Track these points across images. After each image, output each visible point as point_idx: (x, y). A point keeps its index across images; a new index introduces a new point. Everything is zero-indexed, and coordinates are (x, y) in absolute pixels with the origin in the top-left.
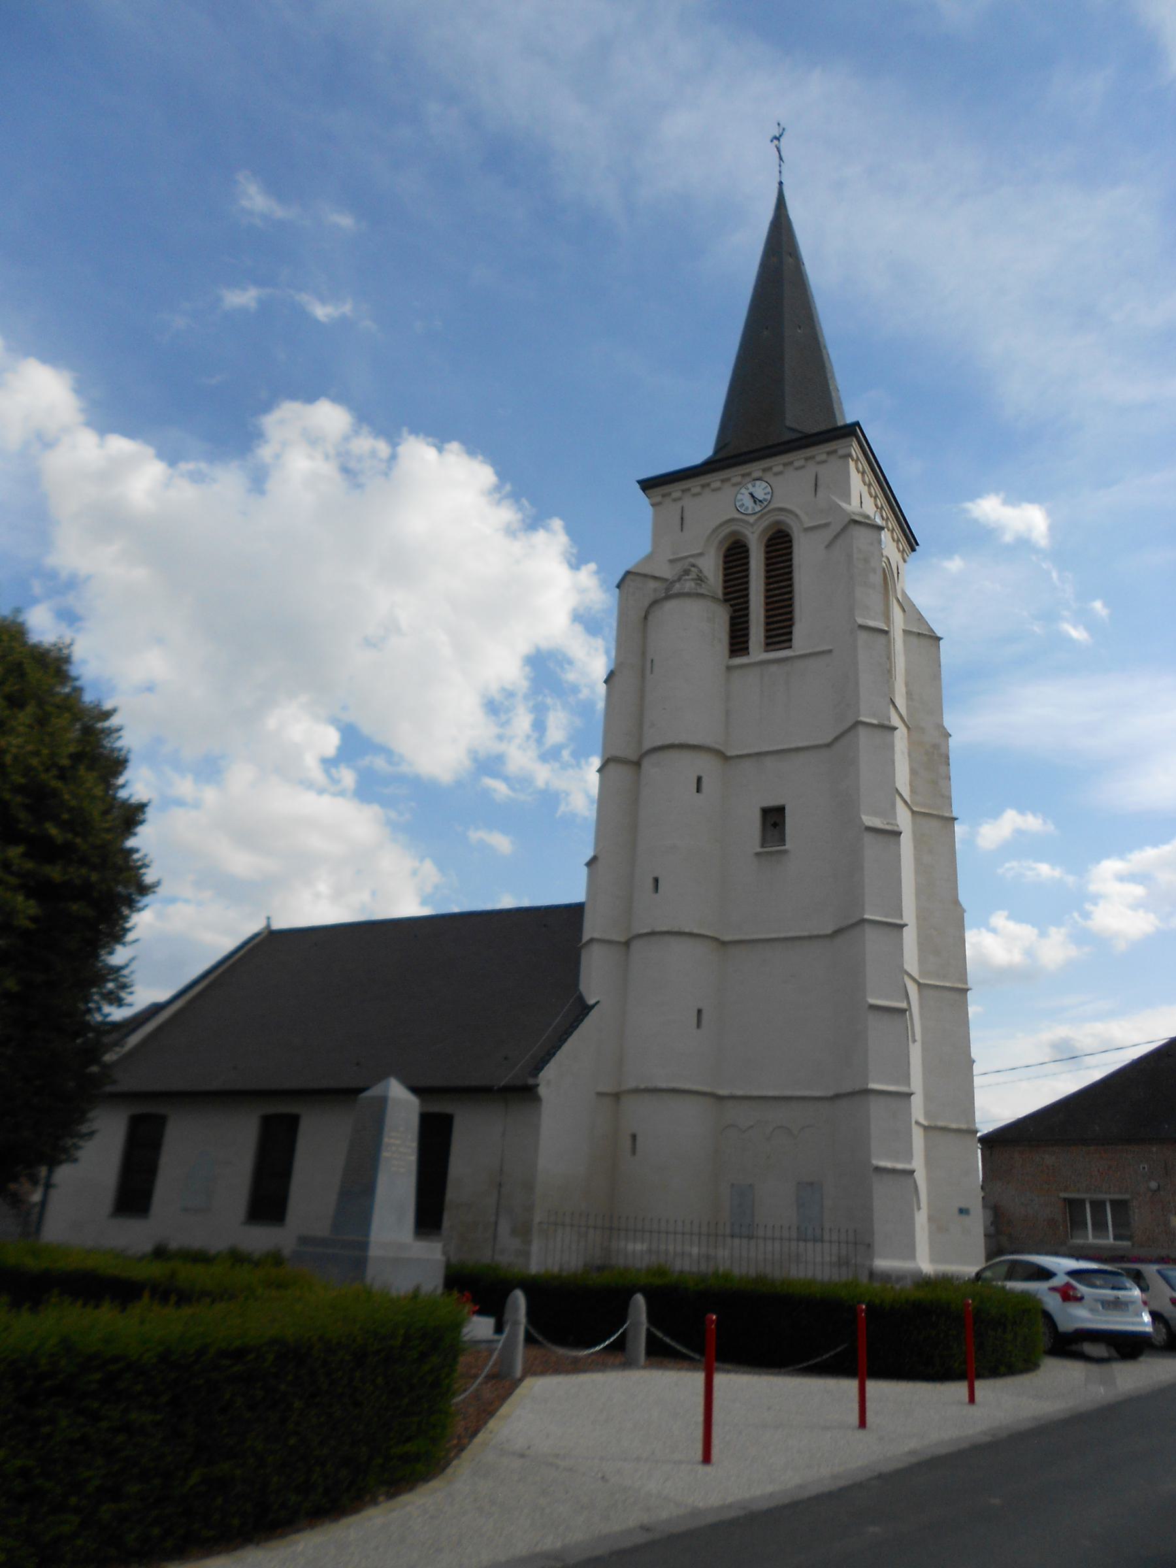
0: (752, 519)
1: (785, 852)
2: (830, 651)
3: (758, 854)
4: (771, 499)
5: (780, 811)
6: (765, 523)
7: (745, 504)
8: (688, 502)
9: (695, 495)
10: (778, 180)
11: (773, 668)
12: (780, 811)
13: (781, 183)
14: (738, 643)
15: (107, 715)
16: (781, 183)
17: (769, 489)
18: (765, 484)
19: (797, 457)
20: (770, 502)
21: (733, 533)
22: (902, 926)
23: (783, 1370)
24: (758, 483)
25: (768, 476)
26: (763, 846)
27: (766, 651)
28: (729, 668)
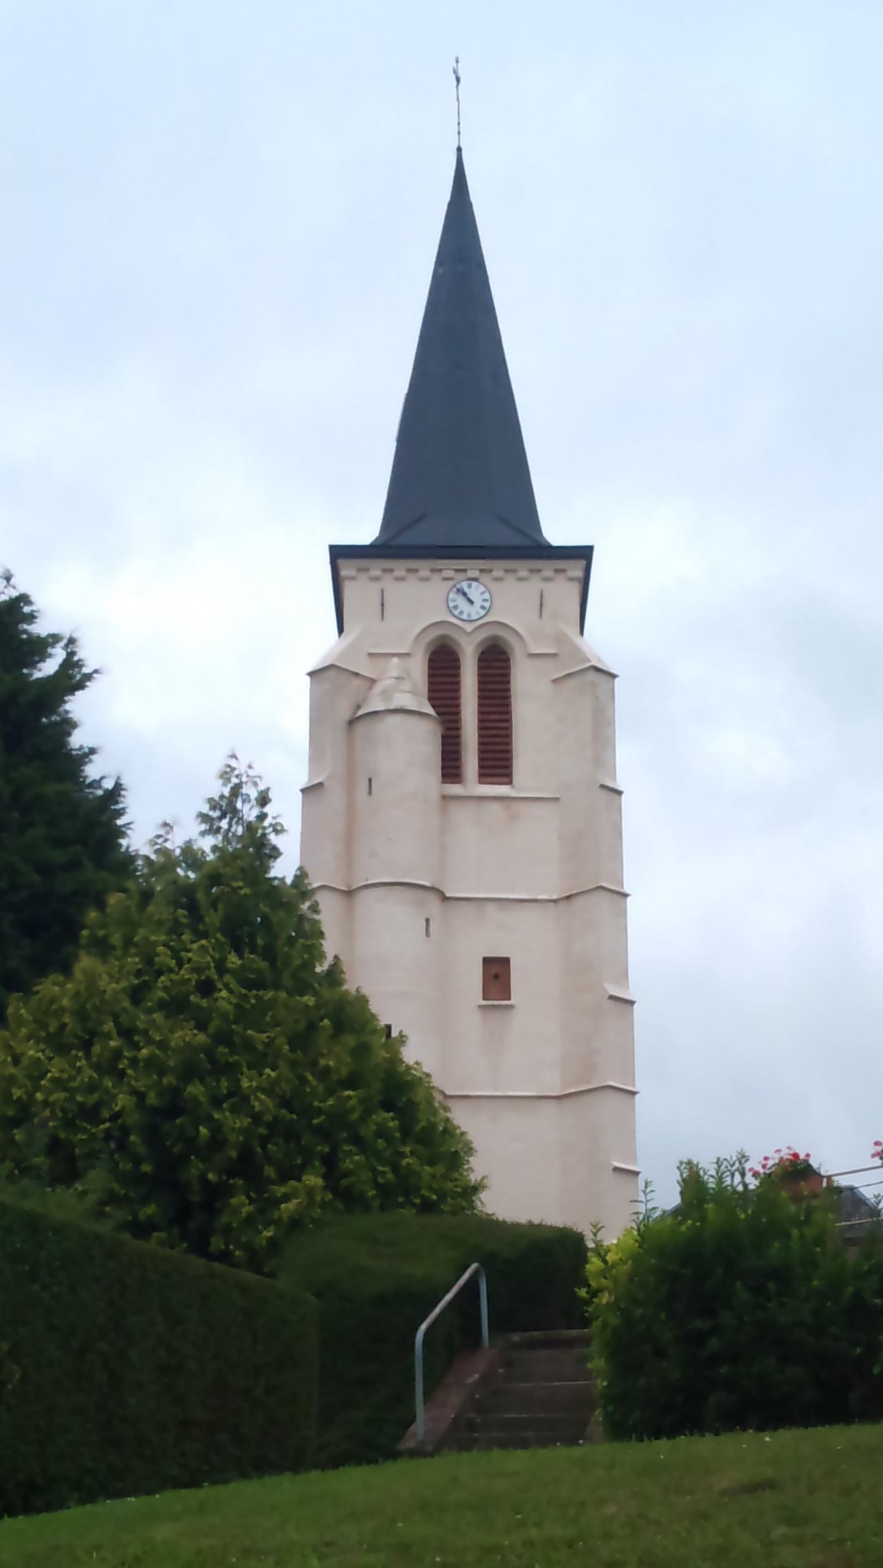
0: (469, 628)
1: (511, 1007)
2: (558, 799)
3: (480, 1007)
4: (490, 607)
5: (505, 962)
6: (482, 635)
7: (459, 605)
8: (388, 583)
9: (398, 579)
10: (456, 146)
11: (495, 807)
12: (505, 962)
13: (459, 150)
14: (451, 769)
15: (124, 789)
16: (459, 150)
17: (487, 596)
18: (482, 588)
19: (523, 567)
20: (488, 611)
21: (444, 637)
22: (634, 1093)
23: (864, 1198)
24: (474, 584)
25: (485, 578)
26: (485, 998)
27: (480, 782)
28: (445, 798)
